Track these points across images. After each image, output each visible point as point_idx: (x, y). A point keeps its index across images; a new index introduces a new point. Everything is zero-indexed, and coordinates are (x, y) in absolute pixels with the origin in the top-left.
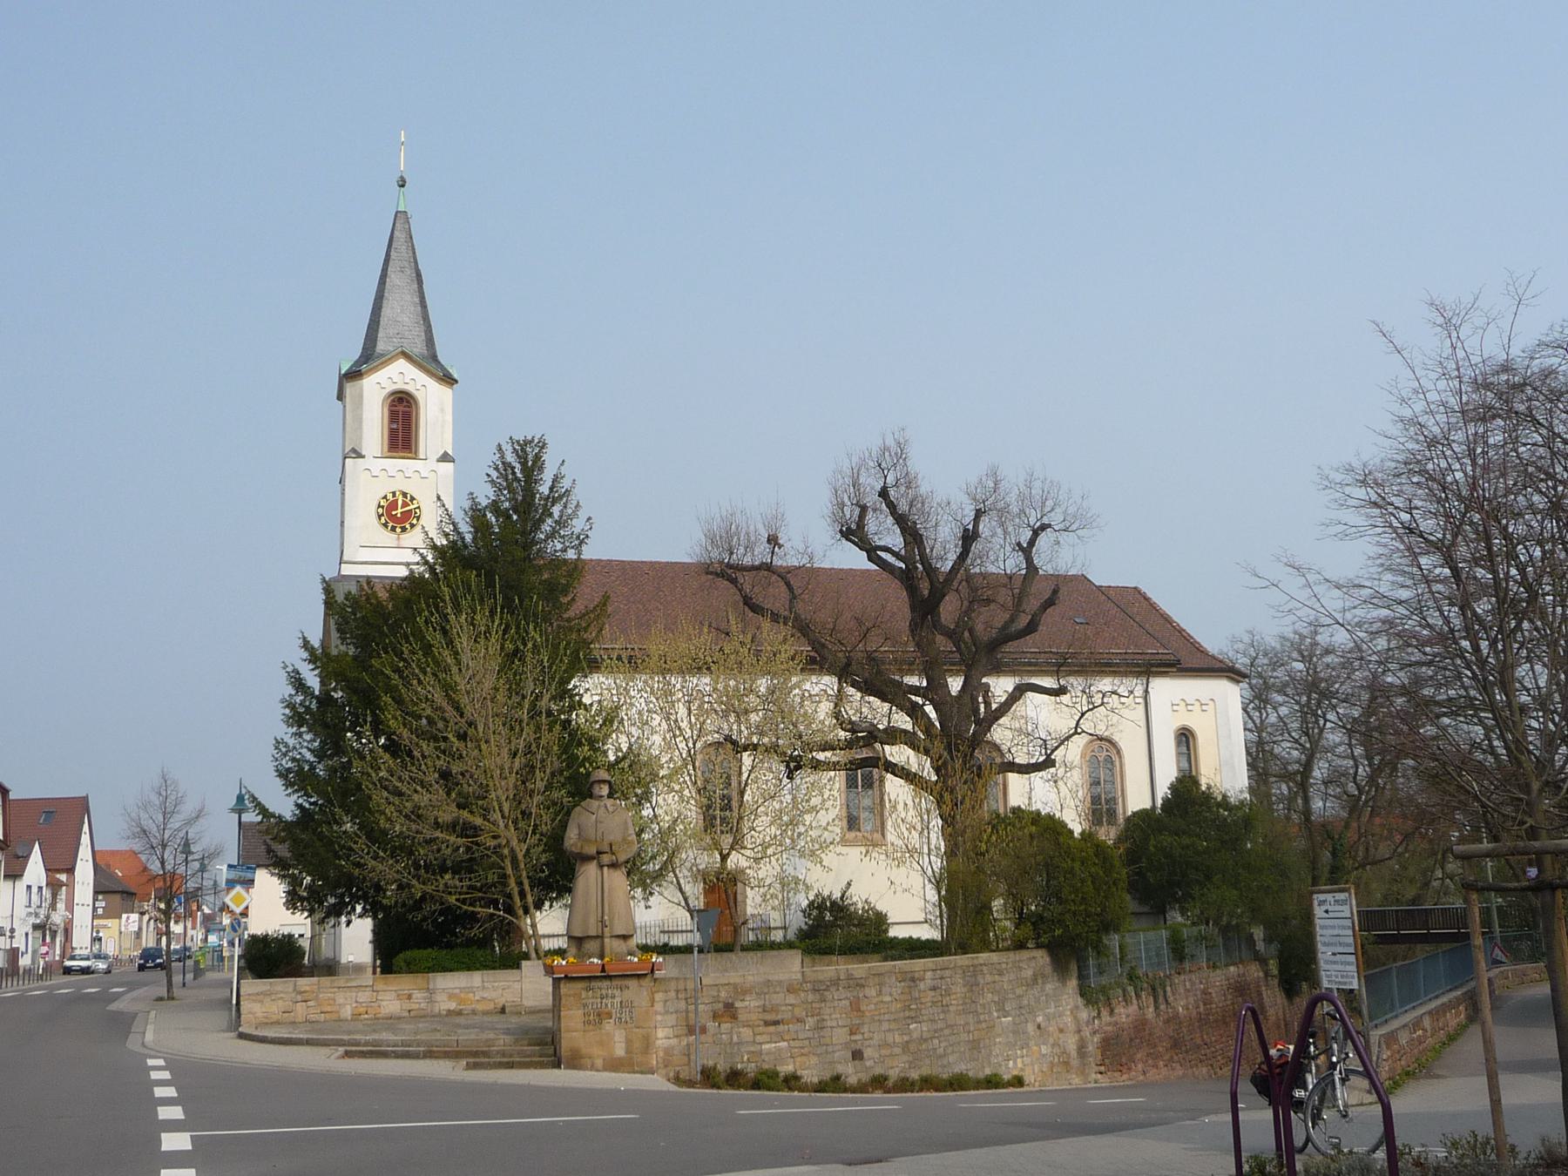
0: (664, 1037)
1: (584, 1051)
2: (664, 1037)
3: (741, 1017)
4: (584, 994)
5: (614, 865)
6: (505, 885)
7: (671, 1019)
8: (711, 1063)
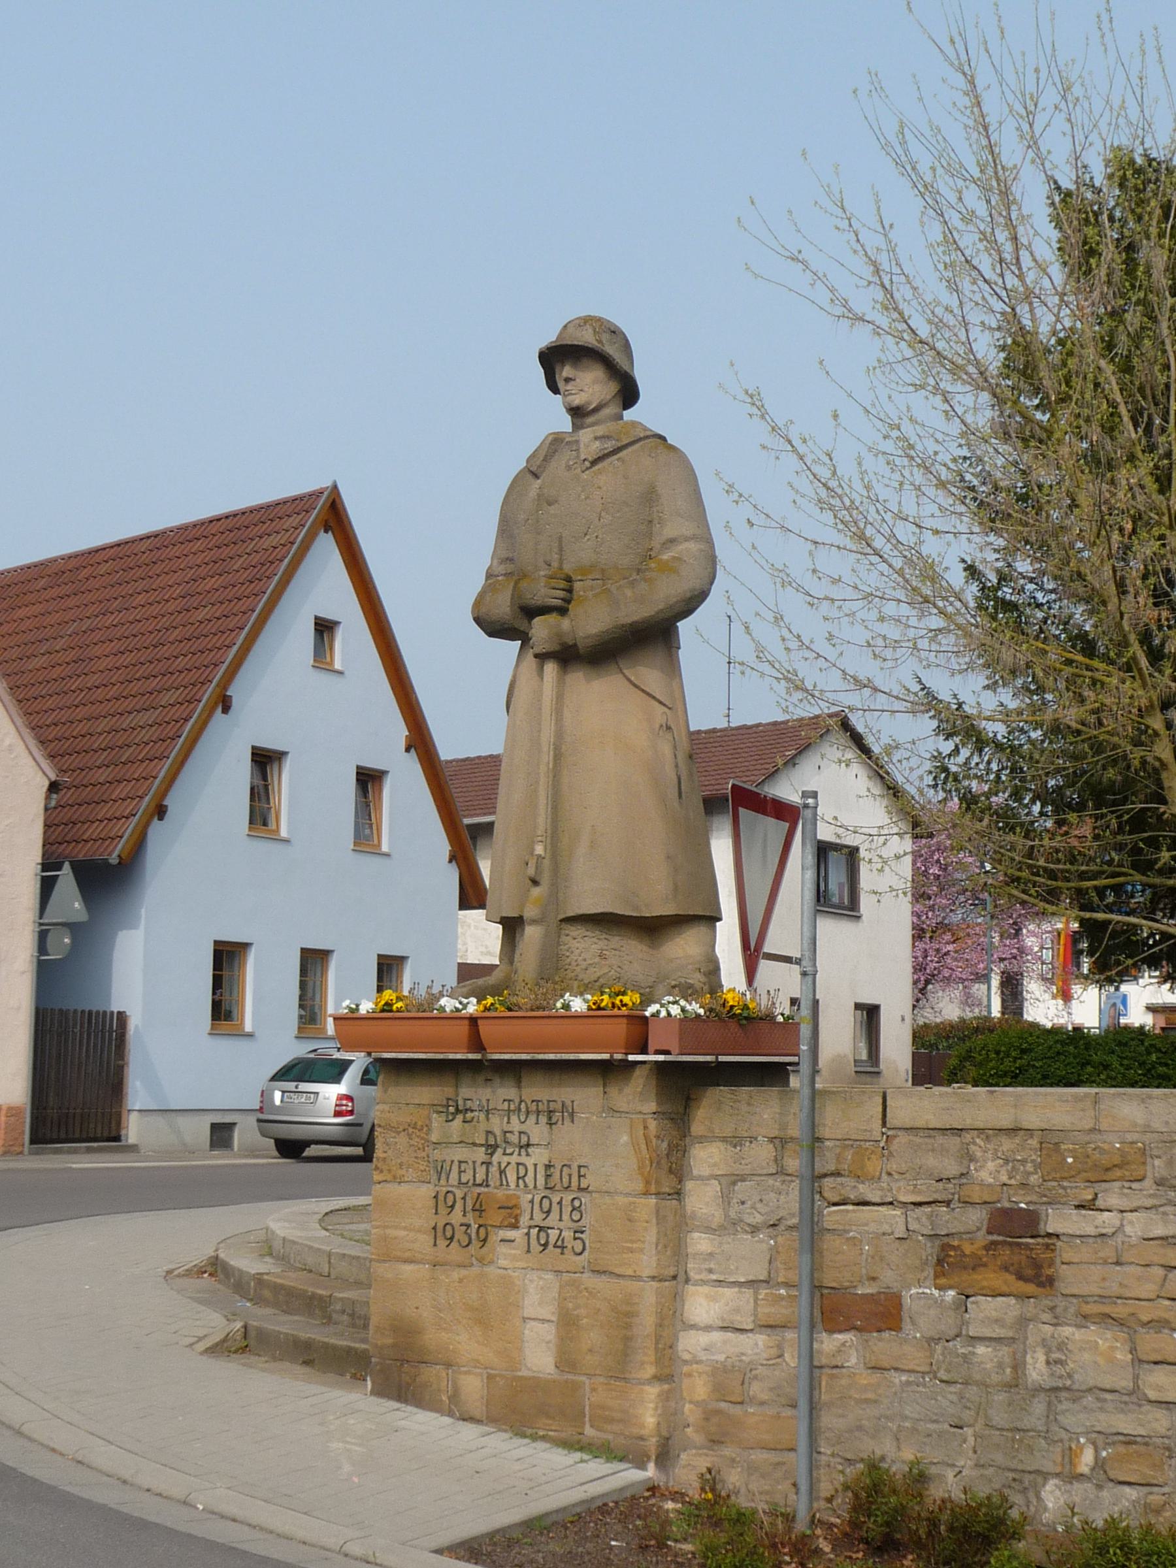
1: (432, 1337)
3: (1079, 1275)
7: (750, 1255)
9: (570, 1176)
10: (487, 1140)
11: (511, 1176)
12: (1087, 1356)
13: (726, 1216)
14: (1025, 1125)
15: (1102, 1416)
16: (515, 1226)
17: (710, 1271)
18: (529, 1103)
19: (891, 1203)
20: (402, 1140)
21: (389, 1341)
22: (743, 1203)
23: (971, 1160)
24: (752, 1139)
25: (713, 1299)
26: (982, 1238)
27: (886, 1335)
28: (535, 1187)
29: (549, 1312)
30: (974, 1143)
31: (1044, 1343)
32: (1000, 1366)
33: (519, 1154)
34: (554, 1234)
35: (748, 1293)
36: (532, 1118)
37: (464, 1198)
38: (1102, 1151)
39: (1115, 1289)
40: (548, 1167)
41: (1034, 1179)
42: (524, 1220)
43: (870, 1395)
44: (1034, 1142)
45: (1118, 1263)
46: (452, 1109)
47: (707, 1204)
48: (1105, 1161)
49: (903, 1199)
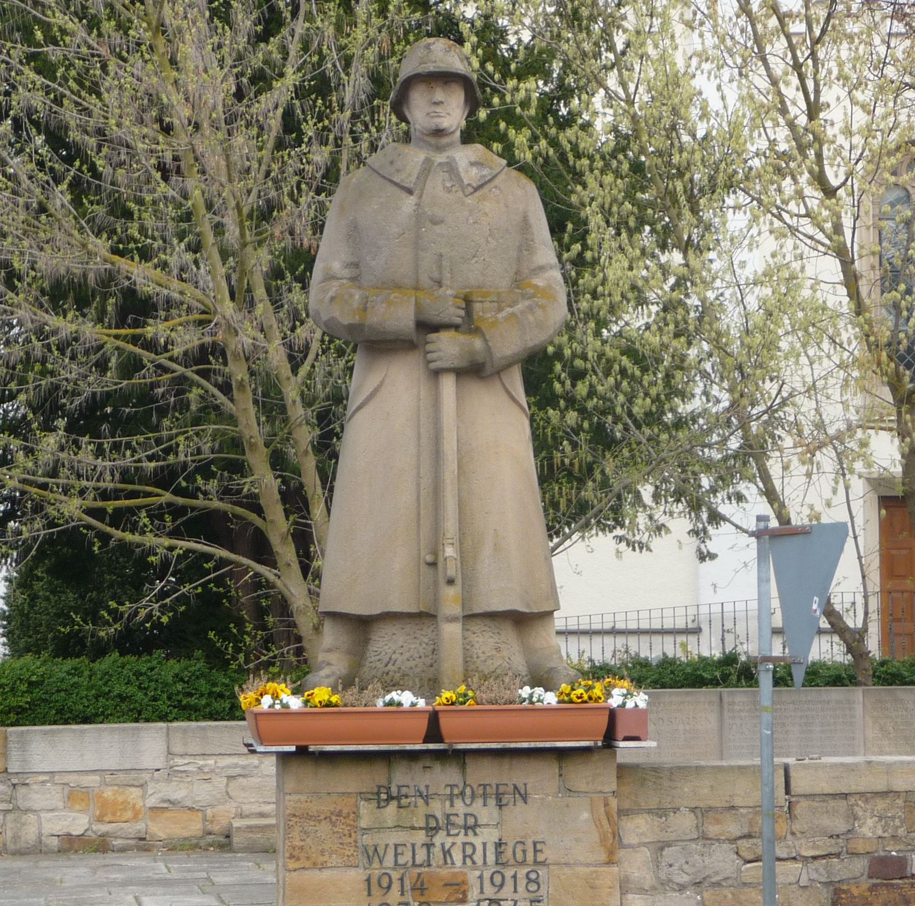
4: (367, 813)
5: (473, 371)
6: (239, 468)
9: (524, 851)
10: (427, 823)
11: (457, 856)
13: (658, 878)
14: (896, 788)
18: (475, 787)
19: (794, 858)
20: (324, 828)
22: (671, 866)
23: (855, 819)
24: (676, 810)
26: (866, 883)
28: (485, 862)
30: (857, 805)
33: (466, 834)
37: (402, 879)
40: (499, 844)
41: (901, 832)
44: (900, 802)
46: (384, 796)
47: (639, 868)
49: (805, 854)
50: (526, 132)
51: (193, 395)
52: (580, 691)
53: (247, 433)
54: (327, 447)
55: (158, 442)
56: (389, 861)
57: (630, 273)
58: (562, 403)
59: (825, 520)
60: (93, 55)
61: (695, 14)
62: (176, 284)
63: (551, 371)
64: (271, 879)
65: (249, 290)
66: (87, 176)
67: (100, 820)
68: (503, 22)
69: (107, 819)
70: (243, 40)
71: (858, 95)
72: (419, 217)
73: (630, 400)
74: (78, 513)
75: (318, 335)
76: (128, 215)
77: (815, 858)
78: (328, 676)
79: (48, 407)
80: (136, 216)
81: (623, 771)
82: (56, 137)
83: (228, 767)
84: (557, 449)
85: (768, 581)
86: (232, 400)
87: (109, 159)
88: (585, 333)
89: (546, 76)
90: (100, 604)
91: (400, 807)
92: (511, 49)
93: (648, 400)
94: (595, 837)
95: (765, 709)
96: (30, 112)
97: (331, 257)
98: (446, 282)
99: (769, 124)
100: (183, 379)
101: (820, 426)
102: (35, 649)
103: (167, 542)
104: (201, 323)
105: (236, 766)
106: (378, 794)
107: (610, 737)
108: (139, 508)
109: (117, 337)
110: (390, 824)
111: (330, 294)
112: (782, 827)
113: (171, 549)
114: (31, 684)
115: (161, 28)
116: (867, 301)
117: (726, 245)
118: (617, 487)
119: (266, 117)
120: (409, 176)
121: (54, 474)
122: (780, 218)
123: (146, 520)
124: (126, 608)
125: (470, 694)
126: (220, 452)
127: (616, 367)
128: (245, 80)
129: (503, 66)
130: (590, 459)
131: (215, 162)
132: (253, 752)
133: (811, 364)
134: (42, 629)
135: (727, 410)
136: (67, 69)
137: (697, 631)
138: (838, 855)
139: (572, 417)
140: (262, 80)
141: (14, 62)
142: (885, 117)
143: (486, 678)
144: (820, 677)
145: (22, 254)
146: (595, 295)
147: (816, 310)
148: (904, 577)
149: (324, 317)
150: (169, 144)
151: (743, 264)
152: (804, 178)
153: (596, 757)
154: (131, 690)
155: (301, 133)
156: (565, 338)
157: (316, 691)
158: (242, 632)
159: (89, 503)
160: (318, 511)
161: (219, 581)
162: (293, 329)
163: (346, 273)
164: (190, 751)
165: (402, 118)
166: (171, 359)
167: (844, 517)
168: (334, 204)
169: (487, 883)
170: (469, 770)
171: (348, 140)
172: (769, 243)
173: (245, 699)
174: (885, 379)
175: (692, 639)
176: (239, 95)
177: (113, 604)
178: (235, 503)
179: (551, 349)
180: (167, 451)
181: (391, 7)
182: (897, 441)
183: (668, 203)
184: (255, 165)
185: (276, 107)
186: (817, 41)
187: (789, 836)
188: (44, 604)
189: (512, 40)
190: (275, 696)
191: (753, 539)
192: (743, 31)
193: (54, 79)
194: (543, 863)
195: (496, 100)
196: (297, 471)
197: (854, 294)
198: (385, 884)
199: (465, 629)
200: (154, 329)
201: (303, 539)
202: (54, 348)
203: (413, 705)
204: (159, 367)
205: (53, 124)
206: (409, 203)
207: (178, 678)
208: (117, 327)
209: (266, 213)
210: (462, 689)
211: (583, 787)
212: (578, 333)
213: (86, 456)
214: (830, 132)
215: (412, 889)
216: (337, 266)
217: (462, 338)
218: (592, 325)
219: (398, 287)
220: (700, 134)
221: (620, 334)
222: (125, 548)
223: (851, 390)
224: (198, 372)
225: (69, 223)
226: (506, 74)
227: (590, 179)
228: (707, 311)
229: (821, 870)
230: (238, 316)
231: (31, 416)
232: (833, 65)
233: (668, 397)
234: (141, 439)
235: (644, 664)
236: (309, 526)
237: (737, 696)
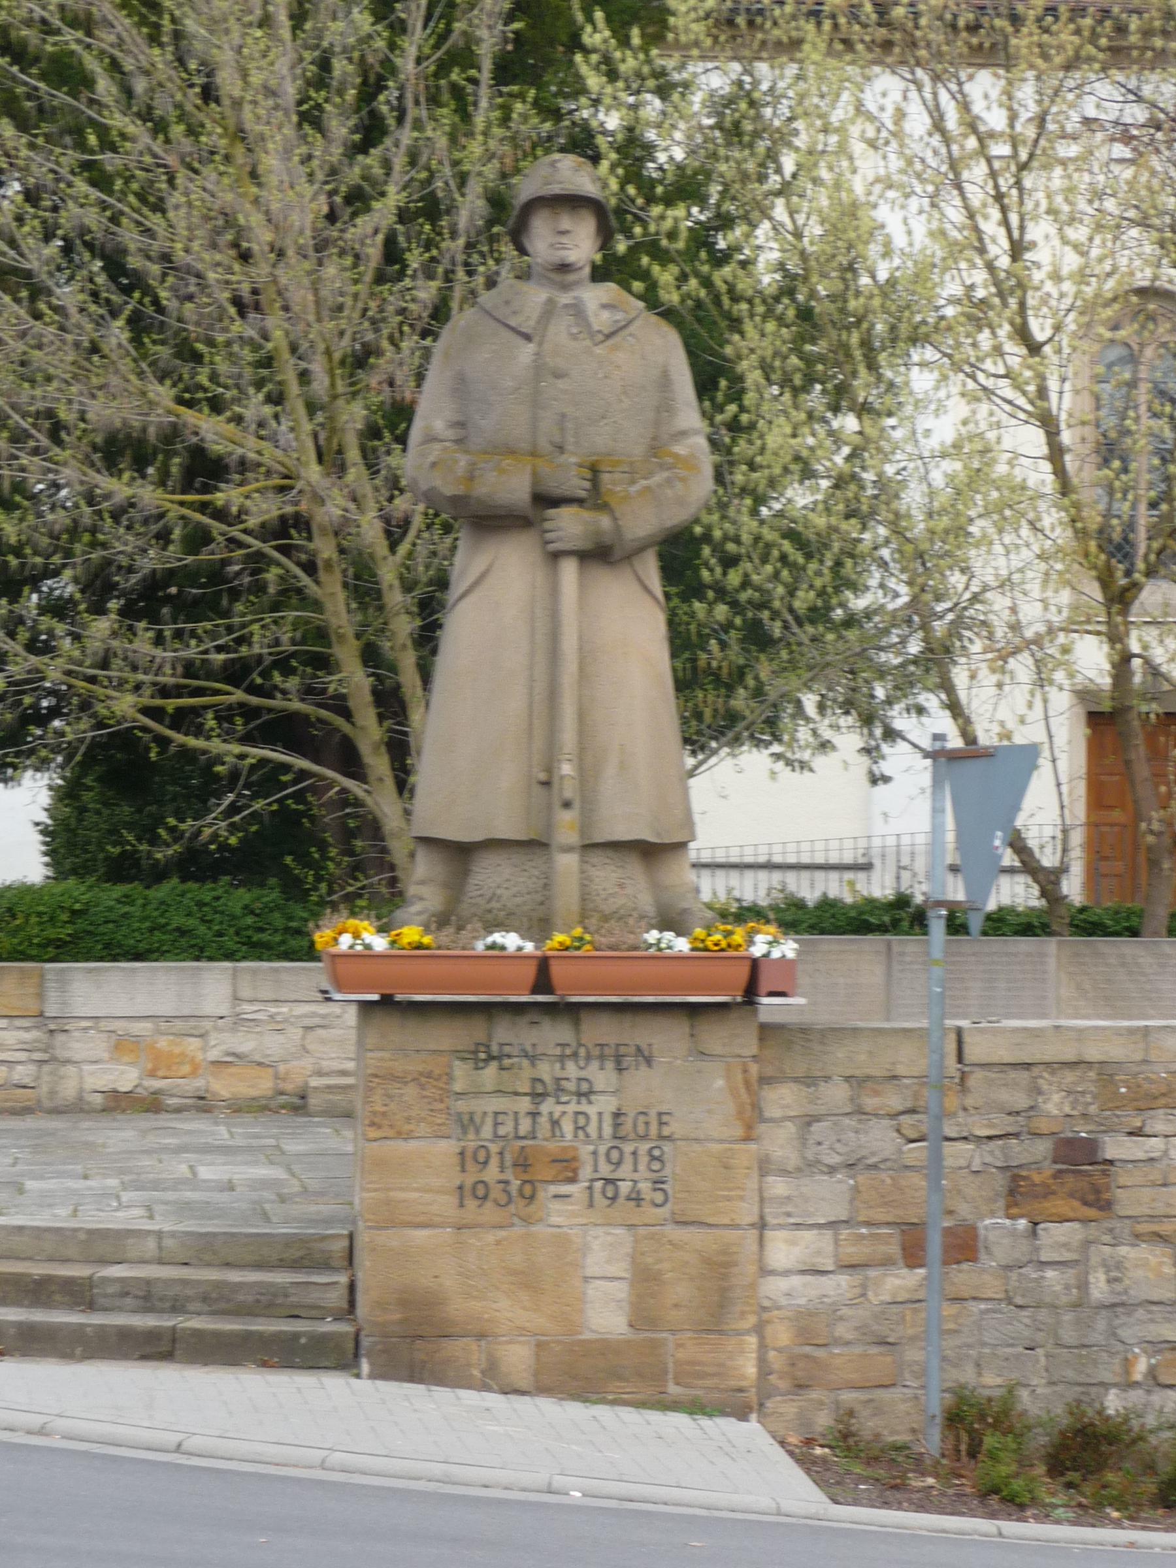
0: (795, 1269)
1: (458, 1307)
2: (795, 1269)
3: (1133, 1198)
5: (599, 554)
6: (323, 663)
8: (991, 1382)
11: (567, 1127)
12: (1140, 1273)
14: (1088, 1058)
15: (1152, 1327)
16: (572, 1180)
17: (789, 1215)
20: (411, 1091)
21: (398, 1316)
24: (827, 1079)
25: (793, 1243)
26: (1049, 1169)
27: (965, 1266)
28: (600, 1137)
29: (620, 1268)
31: (1105, 1264)
32: (1067, 1287)
34: (625, 1187)
35: (828, 1234)
36: (595, 1064)
38: (1151, 1081)
39: (1161, 1209)
40: (617, 1115)
41: (1093, 1109)
42: (586, 1172)
43: (951, 1326)
44: (1092, 1074)
45: (1165, 1185)
48: (1154, 1089)
49: (979, 1133)
50: (674, 269)
51: (271, 575)
52: (717, 937)
53: (334, 622)
54: (428, 638)
55: (230, 629)
56: (487, 1131)
57: (793, 441)
58: (711, 594)
59: (1018, 740)
60: (159, 165)
61: (879, 131)
62: (252, 442)
63: (698, 555)
64: (350, 1148)
65: (340, 452)
66: (150, 310)
67: (152, 1074)
68: (651, 135)
69: (160, 1073)
70: (337, 151)
71: (1071, 233)
72: (539, 369)
73: (792, 593)
74: (131, 713)
75: (421, 507)
76: (197, 358)
77: (990, 1138)
78: (419, 913)
79: (99, 587)
80: (207, 359)
81: (767, 1031)
82: (115, 265)
83: (305, 1016)
84: (704, 650)
85: (943, 811)
86: (317, 582)
87: (172, 289)
88: (739, 511)
89: (702, 200)
90: (160, 821)
91: (502, 1069)
92: (661, 169)
93: (812, 594)
94: (730, 1107)
95: (936, 962)
96: (84, 230)
97: (432, 415)
98: (570, 447)
99: (963, 265)
100: (259, 556)
101: (1015, 627)
102: (79, 871)
103: (237, 749)
104: (282, 489)
105: (314, 1015)
106: (476, 1052)
107: (751, 991)
108: (206, 707)
109: (182, 504)
110: (489, 1088)
111: (431, 459)
112: (952, 1102)
113: (242, 757)
114: (74, 913)
115: (239, 134)
116: (1075, 481)
117: (909, 409)
118: (772, 695)
119: (363, 244)
120: (528, 318)
121: (104, 664)
122: (973, 377)
123: (212, 723)
124: (188, 826)
125: (588, 937)
126: (303, 642)
127: (775, 553)
128: (338, 199)
129: (647, 187)
130: (741, 661)
131: (301, 296)
132: (329, 1000)
133: (1008, 553)
134: (91, 848)
135: (908, 605)
136: (127, 181)
137: (867, 867)
138: (1016, 1135)
139: (721, 611)
140: (360, 199)
141: (64, 172)
142: (1100, 260)
143: (606, 918)
144: (1001, 924)
145: (70, 402)
146: (752, 466)
147: (1012, 490)
148: (1111, 807)
149: (424, 486)
150: (246, 274)
151: (928, 433)
152: (1005, 330)
153: (734, 1015)
154: (191, 922)
155: (405, 266)
156: (715, 517)
157: (405, 930)
158: (325, 857)
159: (146, 701)
160: (416, 716)
161: (299, 796)
162: (391, 499)
163: (450, 434)
164: (261, 996)
165: (522, 251)
166: (245, 531)
167: (1039, 736)
168: (439, 348)
169: (602, 1160)
170: (584, 1027)
171: (461, 274)
172: (959, 409)
173: (321, 937)
174: (1094, 573)
175: (861, 876)
176: (332, 217)
177: (172, 821)
178: (319, 705)
179: (698, 530)
180: (240, 641)
181: (514, 116)
182: (1106, 648)
183: (841, 357)
184: (349, 301)
185: (376, 232)
186: (1023, 167)
187: (961, 1113)
188: (95, 818)
189: (662, 157)
190: (356, 935)
191: (928, 762)
192: (936, 153)
193: (110, 193)
194: (668, 1138)
195: (638, 230)
196: (393, 669)
197: (1060, 472)
198: (481, 1156)
199: (583, 861)
200: (227, 495)
201: (400, 750)
202: (106, 515)
203: (520, 949)
204: (231, 540)
205: (109, 246)
206: (527, 352)
207: (248, 910)
208: (183, 492)
209: (361, 359)
210: (578, 931)
211: (718, 1049)
212: (731, 512)
213: (143, 644)
214: (1037, 276)
215: (515, 1165)
216: (439, 426)
217: (586, 515)
218: (748, 501)
219: (511, 452)
220: (882, 276)
221: (780, 514)
222: (187, 754)
223: (1052, 585)
224: (278, 548)
225: (126, 365)
226: (651, 200)
227: (748, 327)
228: (887, 489)
229: (997, 1153)
230: (326, 482)
231: (78, 596)
232: (1040, 195)
233: (837, 590)
234: (208, 625)
235: (800, 905)
236: (405, 734)
237: (906, 945)
